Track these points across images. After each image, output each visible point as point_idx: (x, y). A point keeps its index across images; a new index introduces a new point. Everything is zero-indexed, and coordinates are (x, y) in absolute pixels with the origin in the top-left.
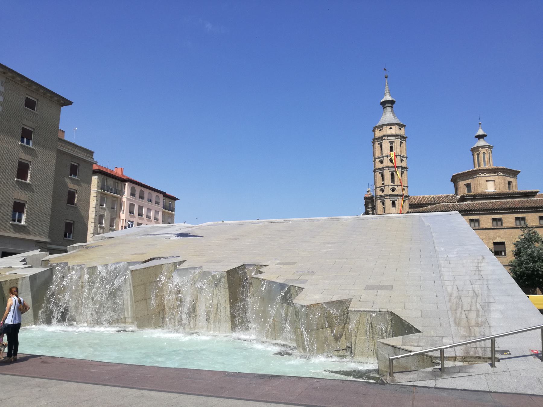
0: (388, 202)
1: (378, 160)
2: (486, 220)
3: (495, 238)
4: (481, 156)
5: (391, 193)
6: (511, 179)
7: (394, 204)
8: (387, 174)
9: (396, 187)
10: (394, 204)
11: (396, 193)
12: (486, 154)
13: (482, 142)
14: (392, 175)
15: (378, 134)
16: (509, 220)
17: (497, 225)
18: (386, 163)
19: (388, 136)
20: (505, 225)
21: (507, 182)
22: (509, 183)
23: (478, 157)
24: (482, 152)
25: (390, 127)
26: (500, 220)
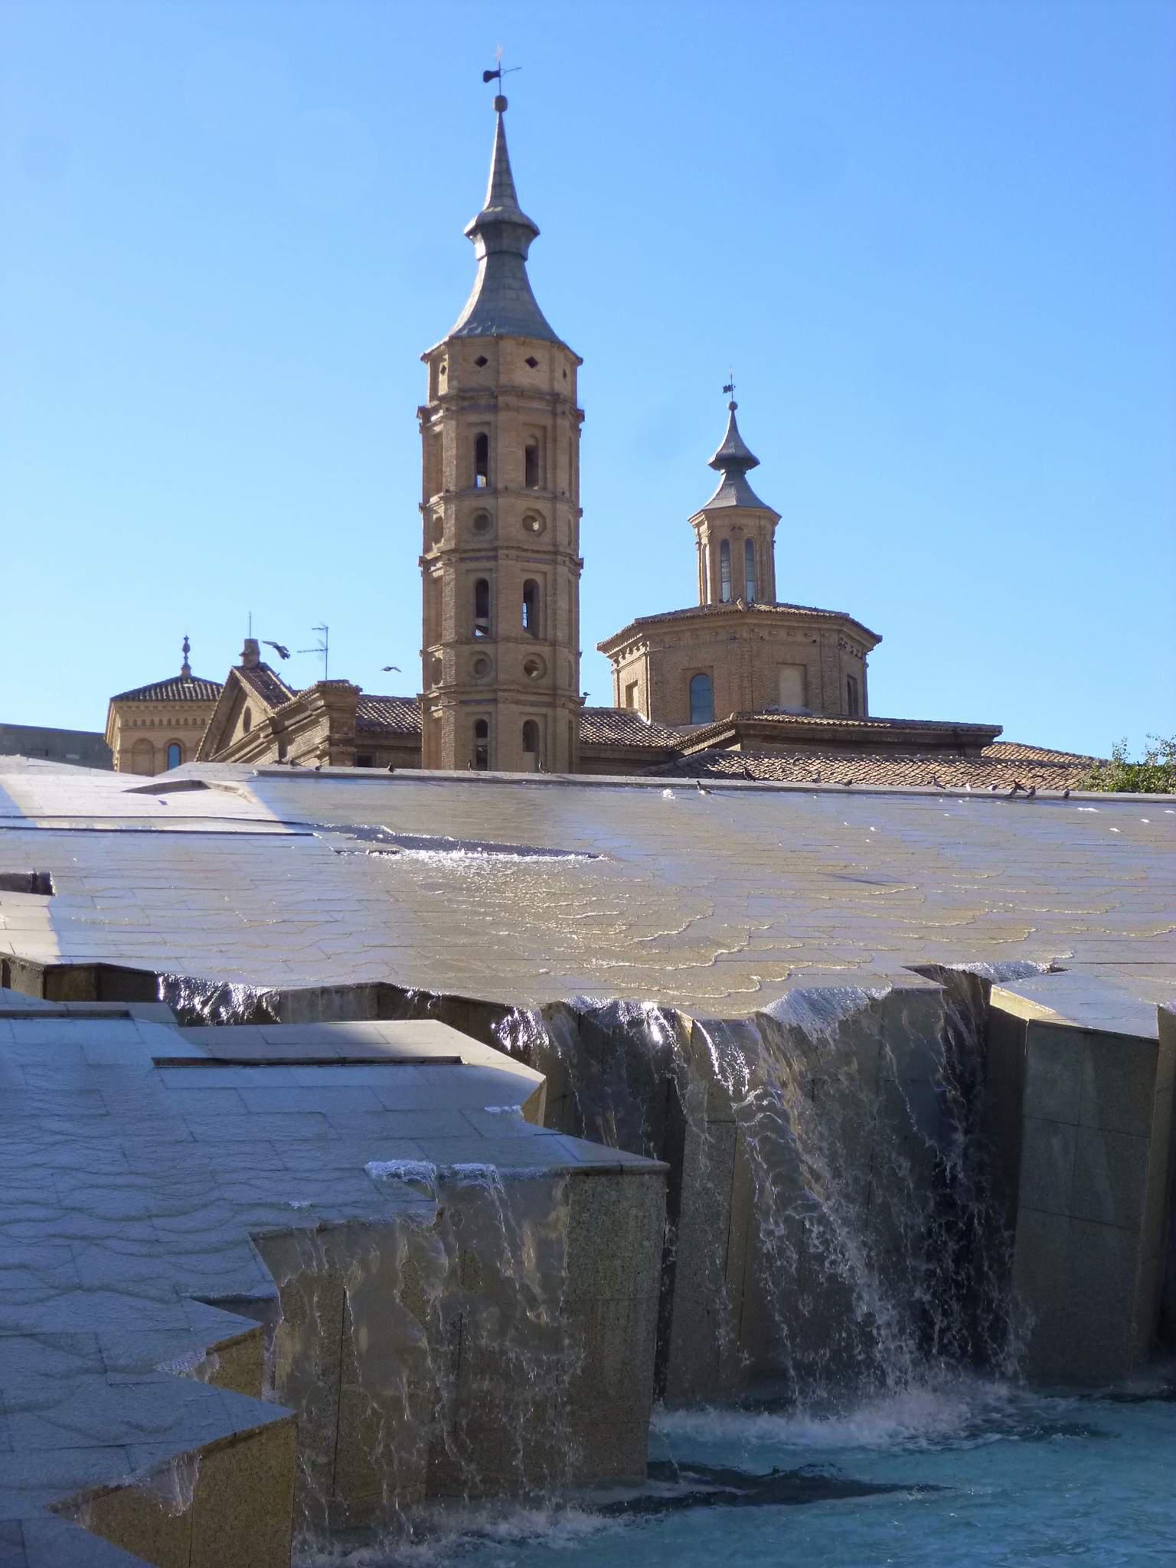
24: (748, 533)
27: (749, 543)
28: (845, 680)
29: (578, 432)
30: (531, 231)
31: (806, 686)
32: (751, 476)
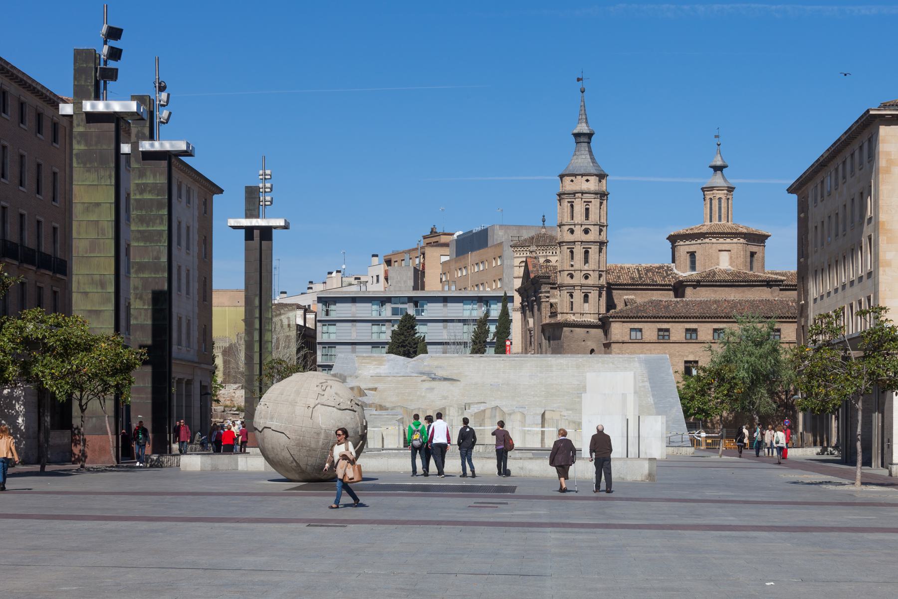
0: (578, 295)
1: (566, 228)
2: (678, 331)
3: (687, 356)
4: (715, 203)
5: (584, 281)
6: (754, 249)
7: (586, 298)
8: (579, 251)
9: (591, 273)
10: (586, 298)
11: (590, 282)
12: (723, 201)
13: (718, 180)
14: (587, 252)
15: (569, 185)
16: (705, 331)
17: (691, 338)
18: (579, 235)
19: (583, 193)
20: (673, 339)
21: (749, 254)
22: (753, 254)
23: (711, 204)
24: (718, 196)
25: (585, 178)
26: (695, 331)
31: (731, 257)
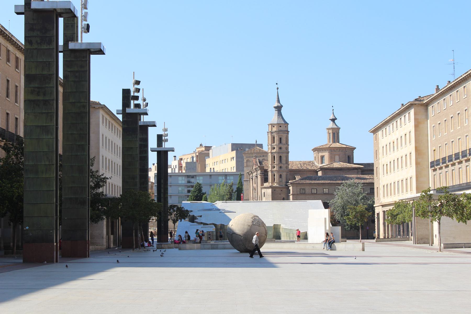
9: (282, 165)
27: (334, 133)
28: (347, 156)
29: (288, 134)
30: (282, 106)
31: (339, 158)
32: (336, 121)
